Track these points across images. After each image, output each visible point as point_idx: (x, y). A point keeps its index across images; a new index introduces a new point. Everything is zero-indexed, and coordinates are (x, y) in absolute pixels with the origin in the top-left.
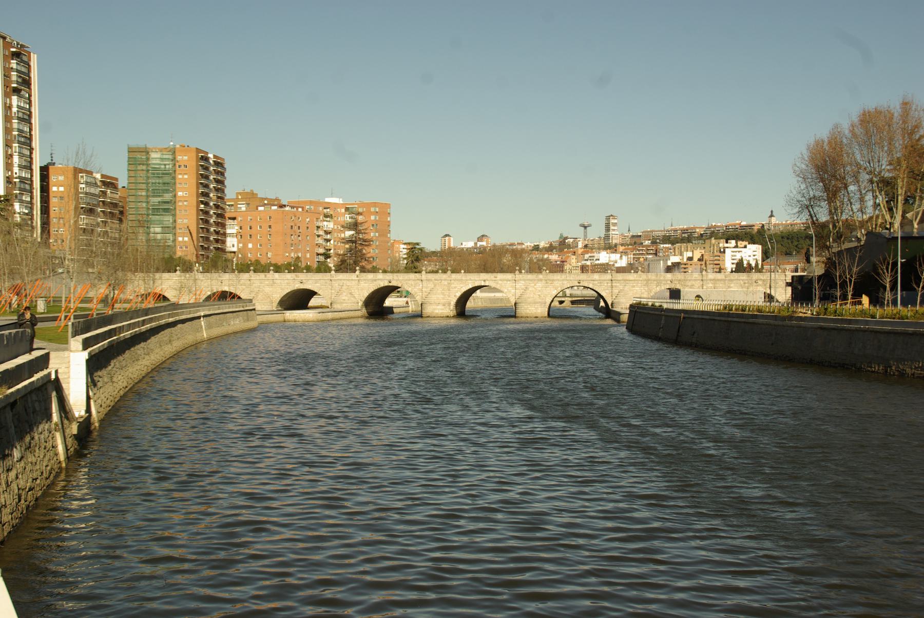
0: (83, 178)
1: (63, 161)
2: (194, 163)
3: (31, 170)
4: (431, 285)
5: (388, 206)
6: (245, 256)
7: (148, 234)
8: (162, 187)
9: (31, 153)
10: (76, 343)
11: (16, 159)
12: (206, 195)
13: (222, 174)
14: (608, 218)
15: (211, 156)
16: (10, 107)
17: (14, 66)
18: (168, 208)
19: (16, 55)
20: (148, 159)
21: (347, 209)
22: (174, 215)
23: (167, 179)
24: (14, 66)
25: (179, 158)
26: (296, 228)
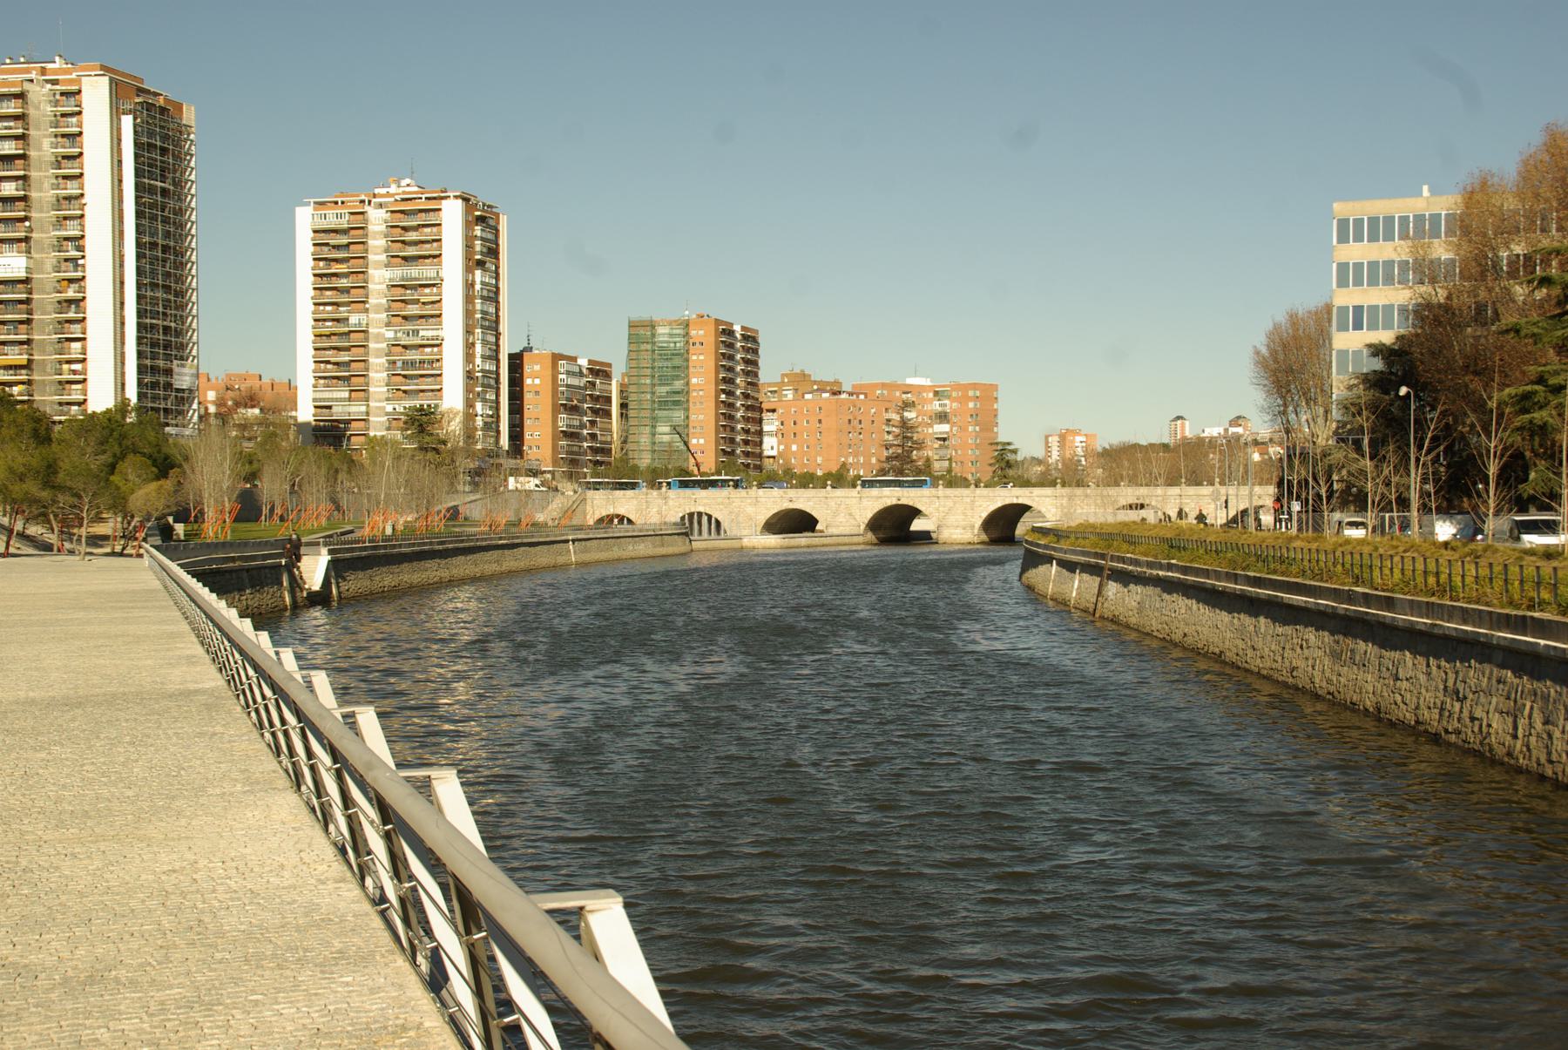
0: (563, 365)
1: (544, 346)
2: (712, 339)
3: (498, 361)
4: (949, 503)
5: (994, 387)
6: (787, 461)
7: (654, 435)
8: (671, 373)
9: (498, 339)
10: (324, 551)
11: (478, 348)
12: (730, 381)
13: (755, 351)
14: (1047, 437)
15: (737, 328)
16: (472, 285)
17: (478, 233)
18: (679, 400)
19: (481, 220)
20: (653, 335)
21: (936, 393)
22: (687, 410)
23: (677, 361)
24: (478, 233)
25: (693, 333)
26: (855, 423)
